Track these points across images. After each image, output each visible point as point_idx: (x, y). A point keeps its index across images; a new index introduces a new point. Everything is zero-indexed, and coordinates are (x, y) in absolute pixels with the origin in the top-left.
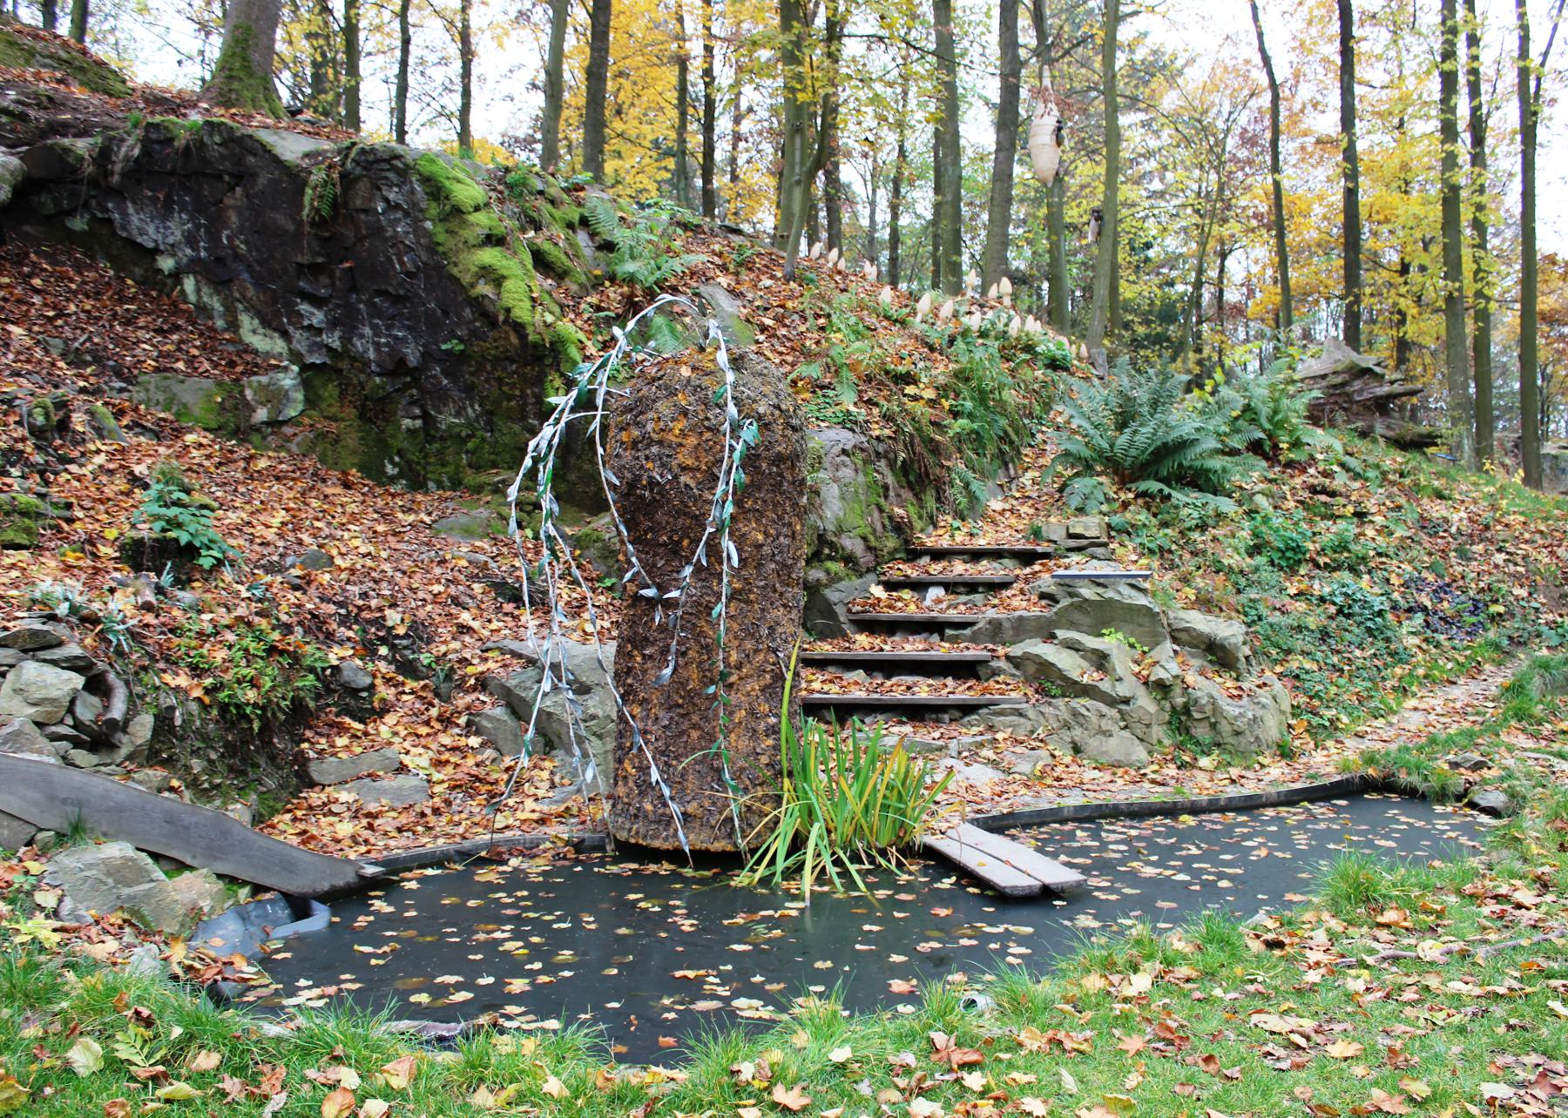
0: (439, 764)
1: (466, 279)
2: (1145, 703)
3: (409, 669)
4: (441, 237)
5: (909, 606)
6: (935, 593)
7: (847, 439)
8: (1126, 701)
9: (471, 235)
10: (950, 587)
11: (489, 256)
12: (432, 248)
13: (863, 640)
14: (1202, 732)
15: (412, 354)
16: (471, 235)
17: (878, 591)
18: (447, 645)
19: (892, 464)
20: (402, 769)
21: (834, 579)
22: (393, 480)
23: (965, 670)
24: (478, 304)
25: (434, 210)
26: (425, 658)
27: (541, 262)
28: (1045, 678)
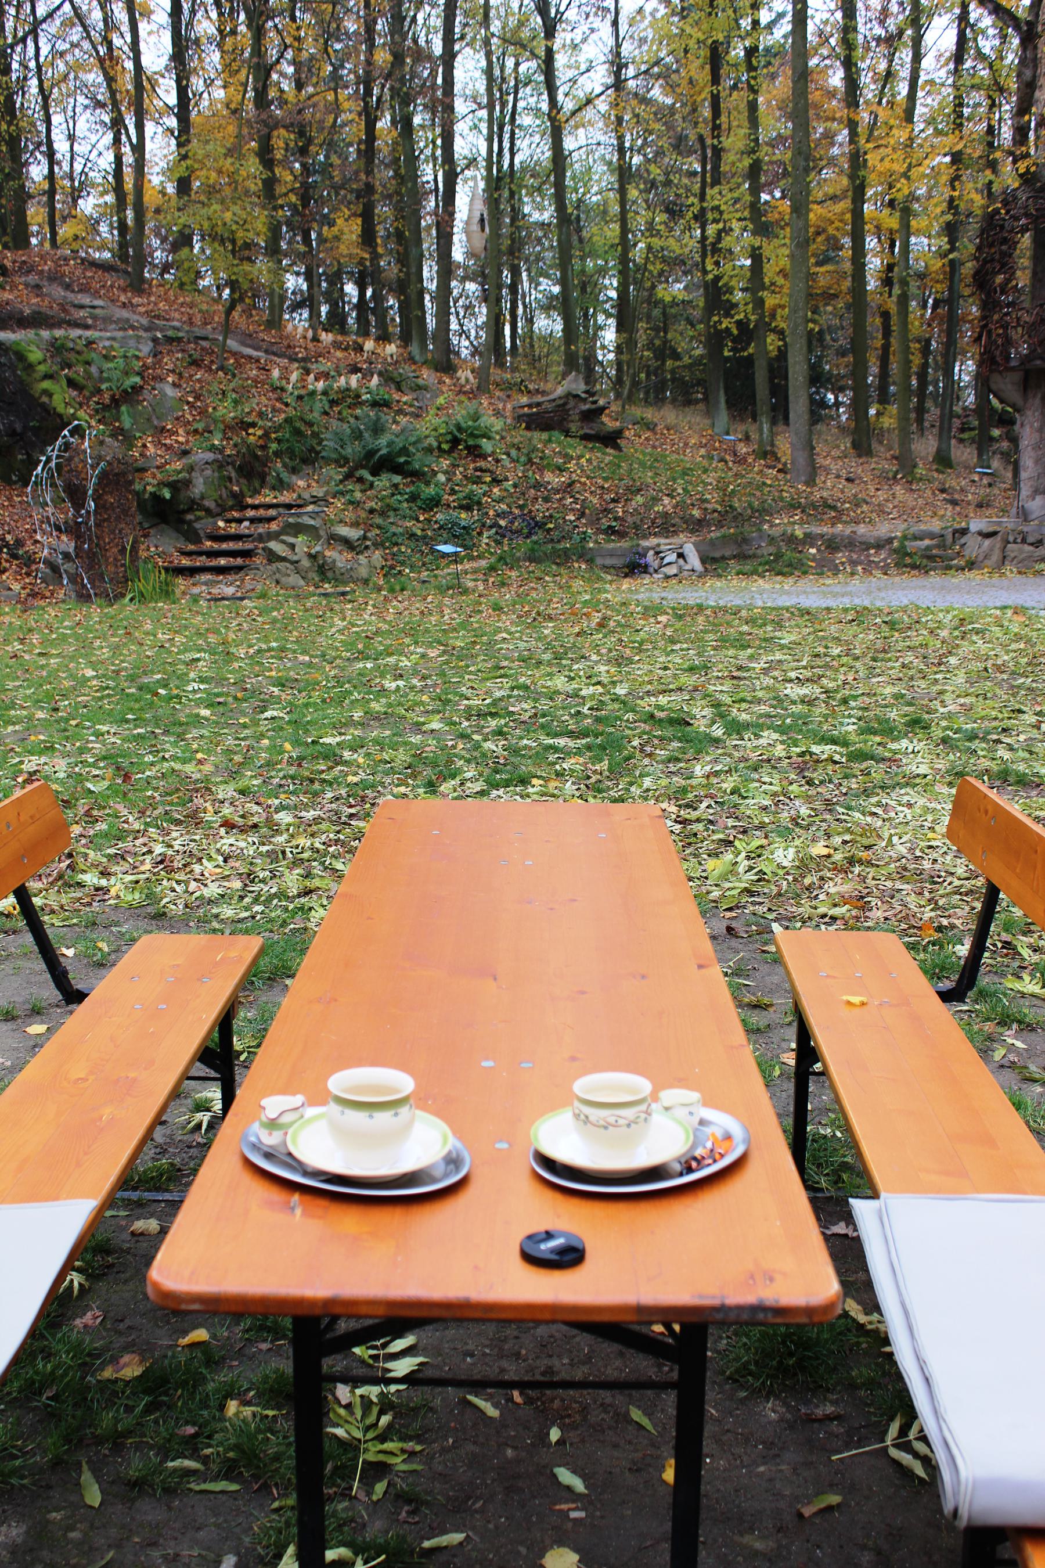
0: (24, 588)
1: (37, 395)
2: (306, 563)
3: (15, 556)
4: (25, 377)
5: (233, 528)
6: (246, 523)
7: (210, 456)
8: (297, 562)
9: (37, 376)
10: (252, 521)
11: (46, 384)
12: (22, 382)
13: (208, 543)
14: (330, 574)
15: (18, 427)
16: (37, 376)
17: (221, 524)
18: (29, 547)
19: (234, 467)
20: (10, 589)
21: (198, 519)
22: (15, 483)
23: (246, 554)
24: (43, 406)
25: (20, 366)
26: (21, 552)
27: (71, 383)
28: (273, 557)
